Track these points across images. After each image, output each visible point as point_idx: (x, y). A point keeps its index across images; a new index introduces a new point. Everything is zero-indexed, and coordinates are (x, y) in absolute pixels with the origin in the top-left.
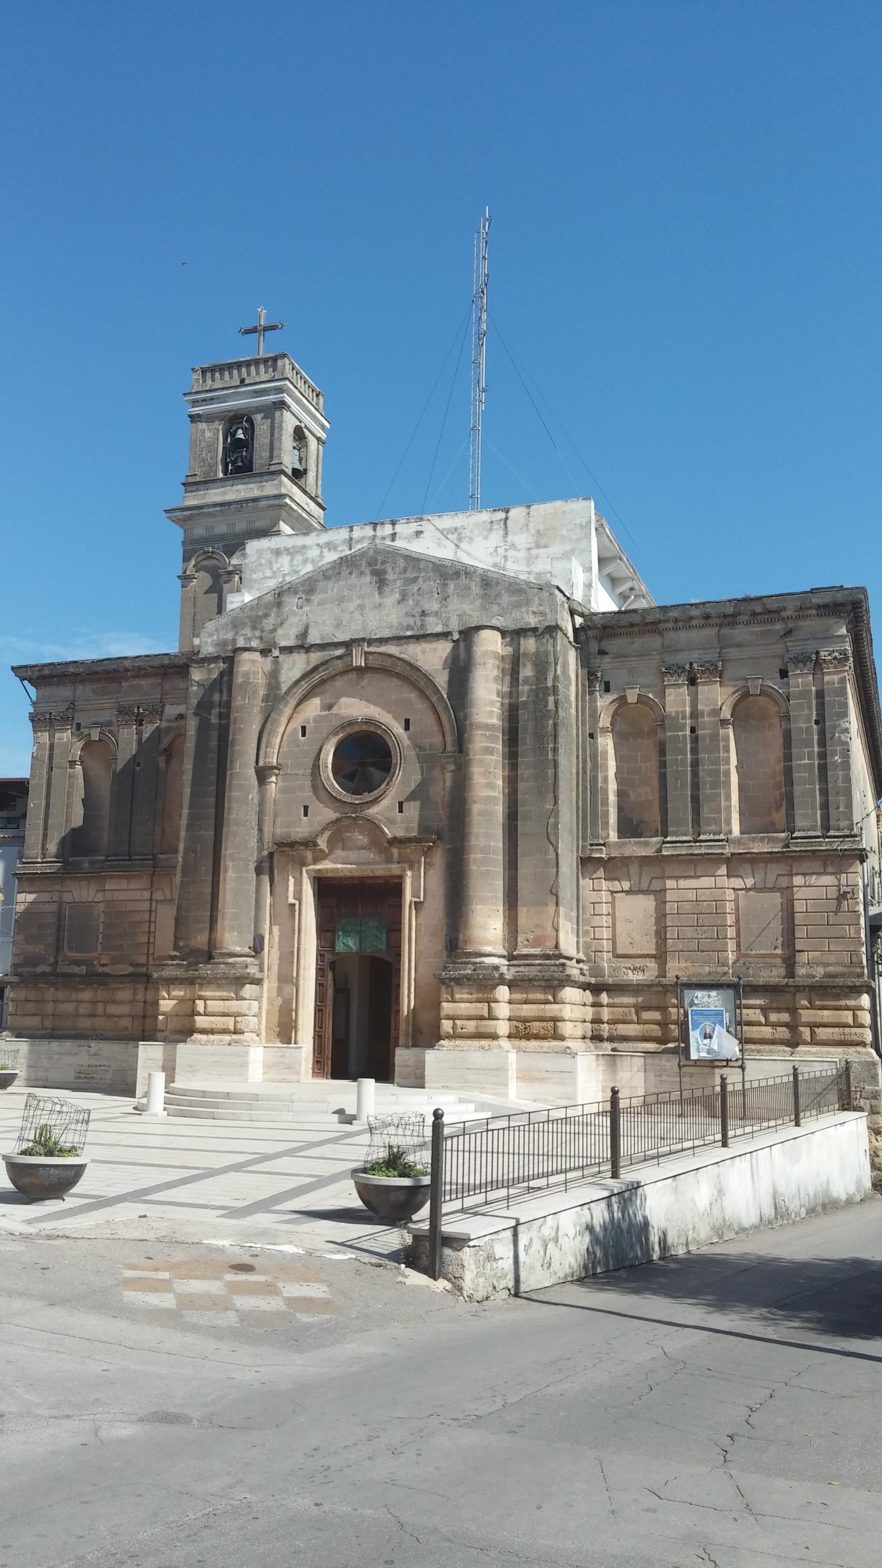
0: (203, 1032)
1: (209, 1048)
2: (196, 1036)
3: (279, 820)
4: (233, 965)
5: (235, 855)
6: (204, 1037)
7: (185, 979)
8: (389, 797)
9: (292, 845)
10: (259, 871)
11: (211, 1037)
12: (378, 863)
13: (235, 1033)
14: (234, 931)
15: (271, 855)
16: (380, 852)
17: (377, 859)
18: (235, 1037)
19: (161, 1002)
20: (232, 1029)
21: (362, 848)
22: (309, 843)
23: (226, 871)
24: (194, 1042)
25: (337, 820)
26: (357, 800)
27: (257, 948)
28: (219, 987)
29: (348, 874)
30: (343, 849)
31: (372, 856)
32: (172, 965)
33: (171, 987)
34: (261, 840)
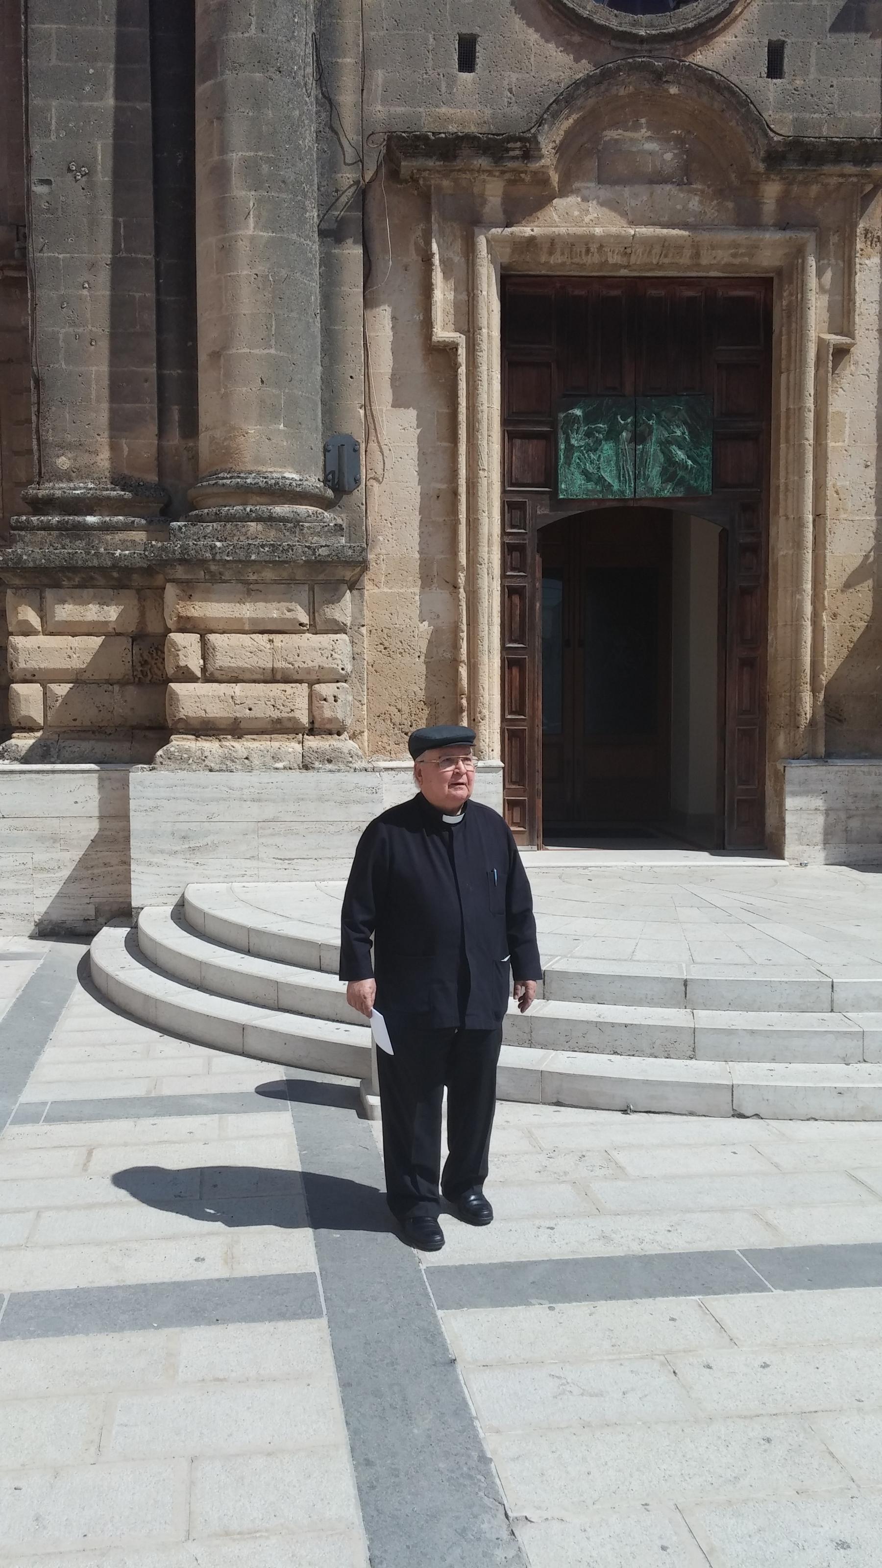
0: (205, 729)
1: (239, 778)
2: (179, 743)
3: (379, 76)
4: (296, 522)
5: (265, 168)
6: (210, 746)
7: (101, 570)
8: (738, 27)
9: (449, 148)
10: (331, 234)
11: (240, 747)
12: (711, 227)
13: (312, 731)
14: (275, 418)
15: (363, 193)
16: (720, 193)
17: (711, 212)
18: (313, 742)
19: (19, 641)
20: (305, 720)
21: (657, 179)
22: (504, 147)
23: (224, 220)
24: (183, 761)
25: (588, 82)
26: (644, 25)
27: (342, 475)
28: (251, 591)
29: (614, 259)
30: (600, 181)
31: (694, 204)
32: (47, 527)
33: (49, 594)
34: (330, 129)
